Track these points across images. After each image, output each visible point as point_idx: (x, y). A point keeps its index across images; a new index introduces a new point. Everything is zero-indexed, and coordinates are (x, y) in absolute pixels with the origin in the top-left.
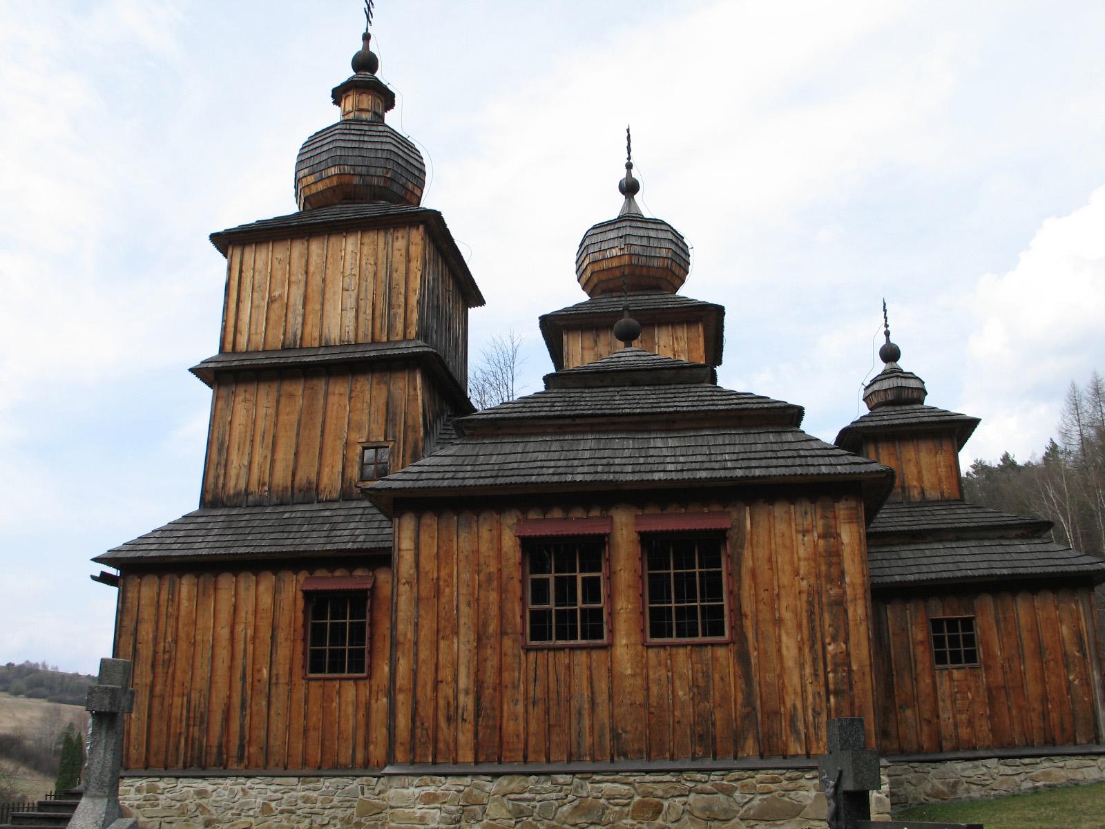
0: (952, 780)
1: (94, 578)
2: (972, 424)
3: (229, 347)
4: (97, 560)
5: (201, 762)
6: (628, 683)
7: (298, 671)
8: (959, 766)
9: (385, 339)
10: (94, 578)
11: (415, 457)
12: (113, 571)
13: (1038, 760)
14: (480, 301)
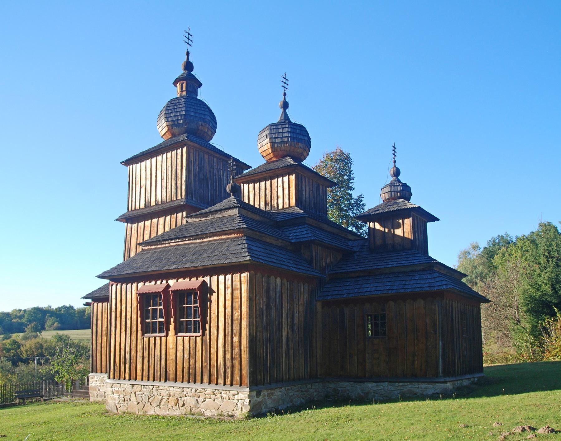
3: (130, 209)
4: (84, 298)
8: (370, 385)
9: (175, 199)
12: (90, 301)
13: (406, 384)
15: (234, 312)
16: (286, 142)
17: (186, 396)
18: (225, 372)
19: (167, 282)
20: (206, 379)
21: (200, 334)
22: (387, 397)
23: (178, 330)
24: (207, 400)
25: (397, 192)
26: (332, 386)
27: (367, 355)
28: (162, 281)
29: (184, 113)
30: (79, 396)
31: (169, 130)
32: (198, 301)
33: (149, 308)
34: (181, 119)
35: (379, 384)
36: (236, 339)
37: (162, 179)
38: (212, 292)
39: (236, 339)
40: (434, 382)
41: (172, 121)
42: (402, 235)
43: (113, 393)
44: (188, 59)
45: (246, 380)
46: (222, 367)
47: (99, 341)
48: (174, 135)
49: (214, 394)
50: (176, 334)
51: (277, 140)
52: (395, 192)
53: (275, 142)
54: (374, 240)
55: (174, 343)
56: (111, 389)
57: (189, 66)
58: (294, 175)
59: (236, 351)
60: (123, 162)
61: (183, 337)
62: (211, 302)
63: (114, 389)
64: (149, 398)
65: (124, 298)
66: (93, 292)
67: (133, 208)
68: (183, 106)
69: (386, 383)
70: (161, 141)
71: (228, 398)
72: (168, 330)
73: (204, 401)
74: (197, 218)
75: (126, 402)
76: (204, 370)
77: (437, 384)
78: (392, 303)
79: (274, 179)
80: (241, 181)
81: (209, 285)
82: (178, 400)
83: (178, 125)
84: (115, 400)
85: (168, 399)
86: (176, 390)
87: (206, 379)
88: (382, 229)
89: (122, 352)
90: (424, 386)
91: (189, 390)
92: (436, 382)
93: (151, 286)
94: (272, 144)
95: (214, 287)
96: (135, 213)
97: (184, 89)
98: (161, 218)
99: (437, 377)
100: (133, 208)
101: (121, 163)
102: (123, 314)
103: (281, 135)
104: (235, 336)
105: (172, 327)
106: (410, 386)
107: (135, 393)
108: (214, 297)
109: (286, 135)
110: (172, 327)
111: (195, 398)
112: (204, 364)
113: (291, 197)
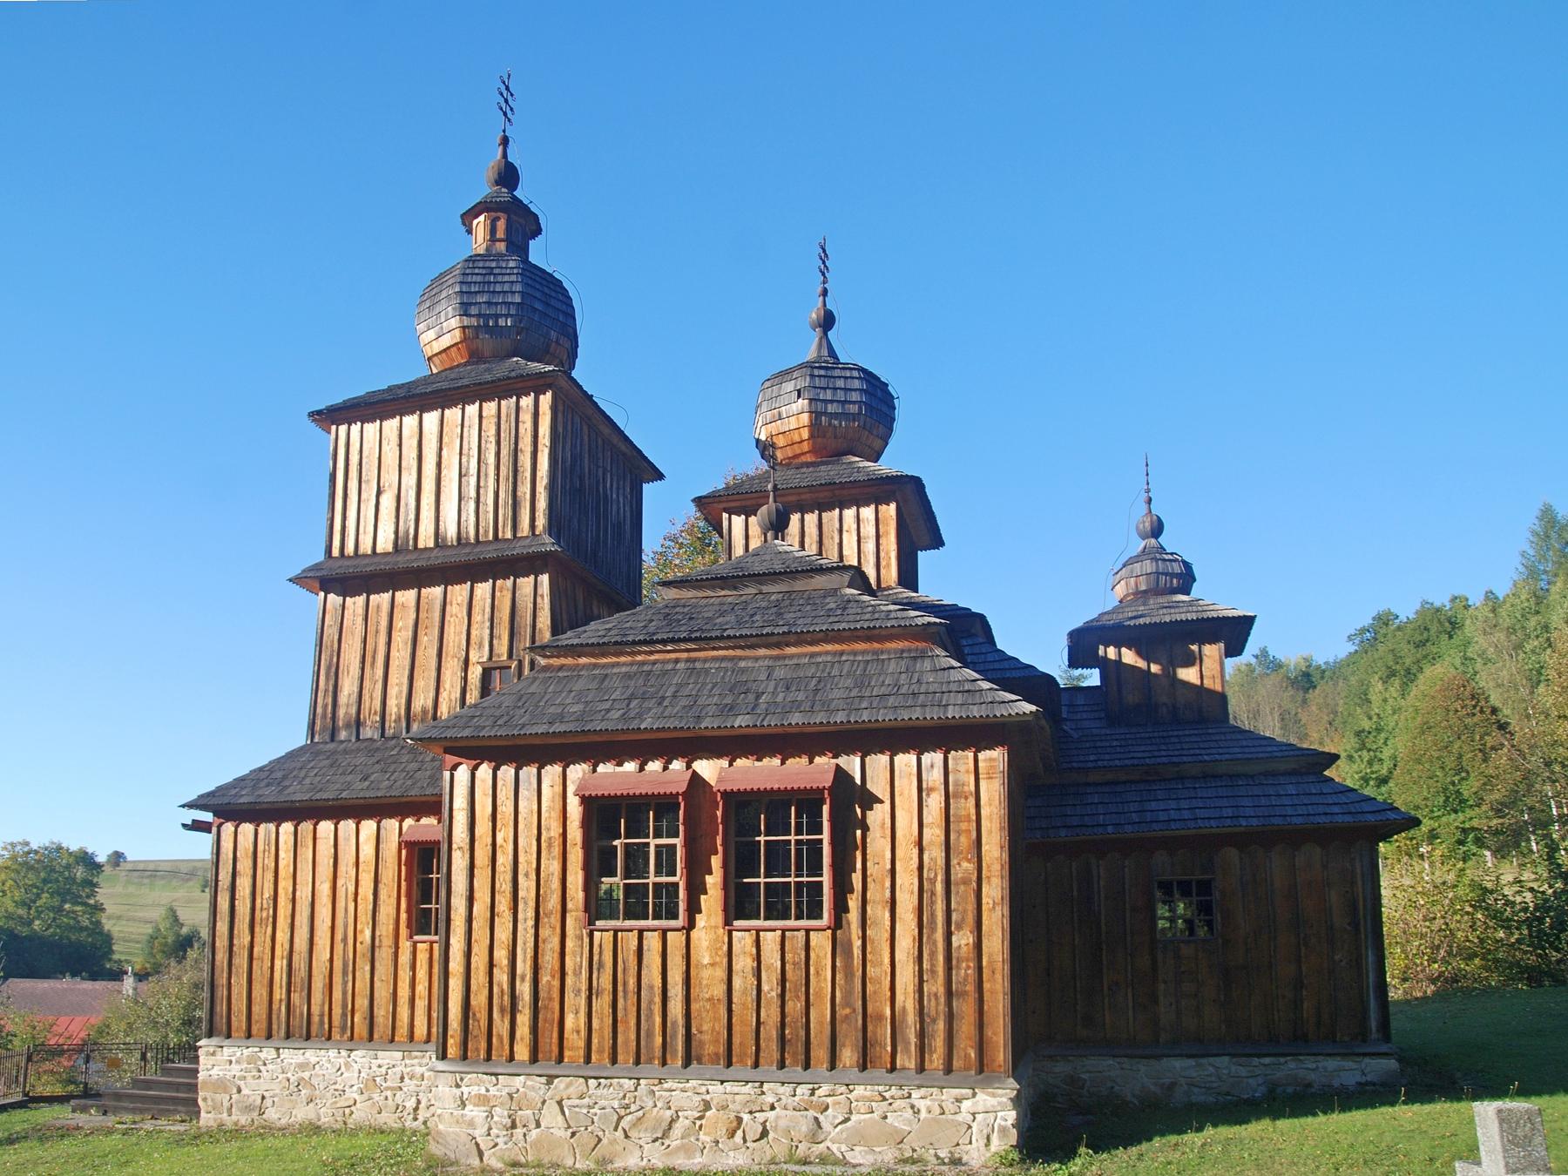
0: (1167, 1081)
1: (184, 826)
2: (1248, 621)
3: (336, 552)
4: (190, 805)
5: (302, 1031)
6: (706, 973)
7: (403, 931)
8: (1178, 1063)
9: (509, 535)
10: (184, 826)
11: (1410, 676)
12: (207, 817)
13: (1282, 1060)
14: (937, 542)
15: (954, 862)
16: (854, 417)
17: (773, 1108)
18: (922, 1034)
19: (689, 767)
20: (848, 1056)
21: (680, 922)
22: (1228, 1094)
23: (739, 905)
24: (854, 1118)
25: (1173, 575)
26: (1062, 1068)
27: (1162, 987)
28: (669, 762)
29: (517, 299)
30: (134, 1111)
31: (464, 340)
32: (681, 828)
33: (616, 843)
34: (507, 316)
35: (1204, 1061)
36: (963, 940)
37: (455, 472)
38: (869, 800)
39: (963, 940)
40: (1359, 1055)
41: (479, 316)
42: (1198, 682)
43: (463, 1105)
44: (505, 155)
45: (1001, 1052)
46: (911, 1018)
47: (243, 938)
48: (475, 357)
49: (885, 1099)
50: (727, 922)
51: (831, 408)
52: (1166, 574)
53: (825, 413)
54: (1119, 691)
55: (715, 948)
56: (457, 1092)
57: (508, 176)
58: (893, 506)
59: (965, 971)
60: (319, 413)
61: (758, 931)
62: (865, 829)
63: (465, 1090)
64: (620, 1118)
65: (506, 809)
66: (219, 789)
67: (350, 549)
68: (513, 278)
69: (1226, 1059)
70: (421, 371)
71: (938, 1111)
72: (694, 908)
73: (847, 1120)
74: (700, 588)
75: (519, 1131)
76: (842, 1028)
77: (1367, 1060)
78: (1232, 854)
79: (831, 509)
80: (722, 506)
81: (858, 782)
82: (739, 1120)
83: (496, 331)
84: (471, 1124)
85: (700, 1118)
86: (736, 1090)
87: (848, 1056)
88: (1142, 664)
89: (501, 977)
90: (1331, 1064)
91: (788, 1089)
92: (1365, 1055)
93: (619, 776)
94: (816, 415)
95: (878, 786)
96: (349, 568)
97: (500, 234)
98: (457, 587)
99: (1364, 1041)
100: (350, 549)
101: (311, 414)
102: (504, 860)
103: (840, 395)
104: (959, 927)
105: (712, 900)
106: (1292, 1065)
107: (560, 1103)
108: (877, 816)
109: (855, 396)
110: (712, 900)
111: (811, 1113)
112: (841, 1012)
113: (883, 563)
